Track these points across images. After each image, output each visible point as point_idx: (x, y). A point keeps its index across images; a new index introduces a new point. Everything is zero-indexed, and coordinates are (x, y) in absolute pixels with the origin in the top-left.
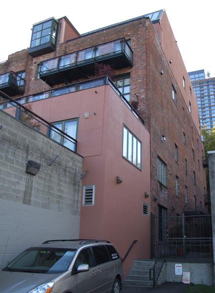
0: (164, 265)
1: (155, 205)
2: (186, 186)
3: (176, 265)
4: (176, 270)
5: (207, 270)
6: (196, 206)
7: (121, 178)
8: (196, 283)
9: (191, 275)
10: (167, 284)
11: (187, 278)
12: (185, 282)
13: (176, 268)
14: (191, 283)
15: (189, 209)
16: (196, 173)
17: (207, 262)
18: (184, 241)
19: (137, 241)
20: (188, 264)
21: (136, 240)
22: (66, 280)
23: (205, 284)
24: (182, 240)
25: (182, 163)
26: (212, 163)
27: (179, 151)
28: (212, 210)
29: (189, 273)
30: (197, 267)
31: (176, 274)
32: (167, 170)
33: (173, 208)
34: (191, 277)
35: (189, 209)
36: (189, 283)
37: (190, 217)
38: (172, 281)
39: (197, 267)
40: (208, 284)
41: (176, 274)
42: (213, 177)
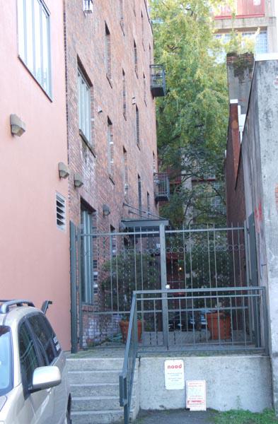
0: (137, 363)
1: (77, 202)
2: (124, 149)
3: (169, 362)
4: (167, 377)
5: (252, 371)
6: (140, 205)
7: (24, 122)
8: (221, 409)
9: (208, 388)
10: (145, 414)
11: (198, 400)
12: (192, 409)
13: (167, 371)
14: (209, 409)
15: (130, 212)
16: (140, 112)
17: (251, 352)
18: (165, 299)
19: (50, 303)
20: (199, 361)
21: (34, 303)
22: (21, 412)
23: (245, 409)
24: (160, 295)
25: (117, 82)
26: (268, 88)
27: (112, 47)
28: (266, 213)
29: (203, 383)
30: (224, 366)
31: (168, 387)
32: (92, 99)
33: (104, 206)
34: (208, 393)
35: (130, 212)
36: (203, 408)
37: (131, 236)
38: (158, 408)
39: (224, 366)
40: (253, 410)
41: (168, 387)
42: (269, 126)
